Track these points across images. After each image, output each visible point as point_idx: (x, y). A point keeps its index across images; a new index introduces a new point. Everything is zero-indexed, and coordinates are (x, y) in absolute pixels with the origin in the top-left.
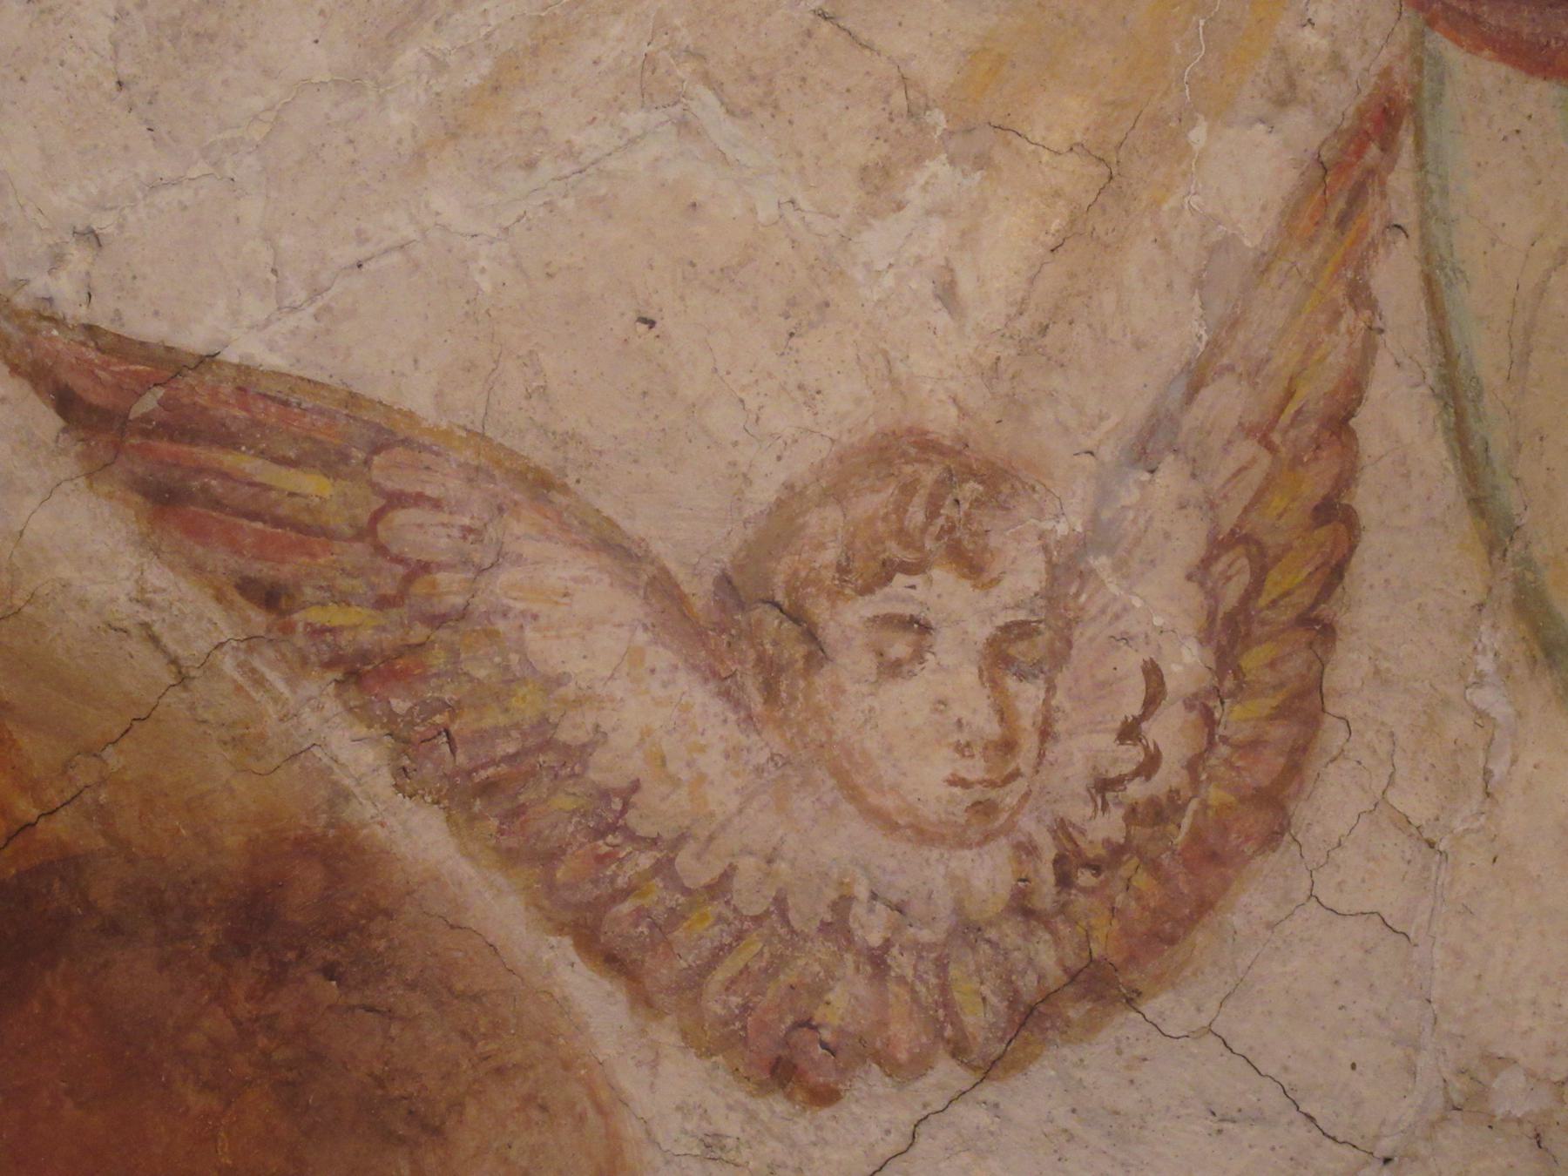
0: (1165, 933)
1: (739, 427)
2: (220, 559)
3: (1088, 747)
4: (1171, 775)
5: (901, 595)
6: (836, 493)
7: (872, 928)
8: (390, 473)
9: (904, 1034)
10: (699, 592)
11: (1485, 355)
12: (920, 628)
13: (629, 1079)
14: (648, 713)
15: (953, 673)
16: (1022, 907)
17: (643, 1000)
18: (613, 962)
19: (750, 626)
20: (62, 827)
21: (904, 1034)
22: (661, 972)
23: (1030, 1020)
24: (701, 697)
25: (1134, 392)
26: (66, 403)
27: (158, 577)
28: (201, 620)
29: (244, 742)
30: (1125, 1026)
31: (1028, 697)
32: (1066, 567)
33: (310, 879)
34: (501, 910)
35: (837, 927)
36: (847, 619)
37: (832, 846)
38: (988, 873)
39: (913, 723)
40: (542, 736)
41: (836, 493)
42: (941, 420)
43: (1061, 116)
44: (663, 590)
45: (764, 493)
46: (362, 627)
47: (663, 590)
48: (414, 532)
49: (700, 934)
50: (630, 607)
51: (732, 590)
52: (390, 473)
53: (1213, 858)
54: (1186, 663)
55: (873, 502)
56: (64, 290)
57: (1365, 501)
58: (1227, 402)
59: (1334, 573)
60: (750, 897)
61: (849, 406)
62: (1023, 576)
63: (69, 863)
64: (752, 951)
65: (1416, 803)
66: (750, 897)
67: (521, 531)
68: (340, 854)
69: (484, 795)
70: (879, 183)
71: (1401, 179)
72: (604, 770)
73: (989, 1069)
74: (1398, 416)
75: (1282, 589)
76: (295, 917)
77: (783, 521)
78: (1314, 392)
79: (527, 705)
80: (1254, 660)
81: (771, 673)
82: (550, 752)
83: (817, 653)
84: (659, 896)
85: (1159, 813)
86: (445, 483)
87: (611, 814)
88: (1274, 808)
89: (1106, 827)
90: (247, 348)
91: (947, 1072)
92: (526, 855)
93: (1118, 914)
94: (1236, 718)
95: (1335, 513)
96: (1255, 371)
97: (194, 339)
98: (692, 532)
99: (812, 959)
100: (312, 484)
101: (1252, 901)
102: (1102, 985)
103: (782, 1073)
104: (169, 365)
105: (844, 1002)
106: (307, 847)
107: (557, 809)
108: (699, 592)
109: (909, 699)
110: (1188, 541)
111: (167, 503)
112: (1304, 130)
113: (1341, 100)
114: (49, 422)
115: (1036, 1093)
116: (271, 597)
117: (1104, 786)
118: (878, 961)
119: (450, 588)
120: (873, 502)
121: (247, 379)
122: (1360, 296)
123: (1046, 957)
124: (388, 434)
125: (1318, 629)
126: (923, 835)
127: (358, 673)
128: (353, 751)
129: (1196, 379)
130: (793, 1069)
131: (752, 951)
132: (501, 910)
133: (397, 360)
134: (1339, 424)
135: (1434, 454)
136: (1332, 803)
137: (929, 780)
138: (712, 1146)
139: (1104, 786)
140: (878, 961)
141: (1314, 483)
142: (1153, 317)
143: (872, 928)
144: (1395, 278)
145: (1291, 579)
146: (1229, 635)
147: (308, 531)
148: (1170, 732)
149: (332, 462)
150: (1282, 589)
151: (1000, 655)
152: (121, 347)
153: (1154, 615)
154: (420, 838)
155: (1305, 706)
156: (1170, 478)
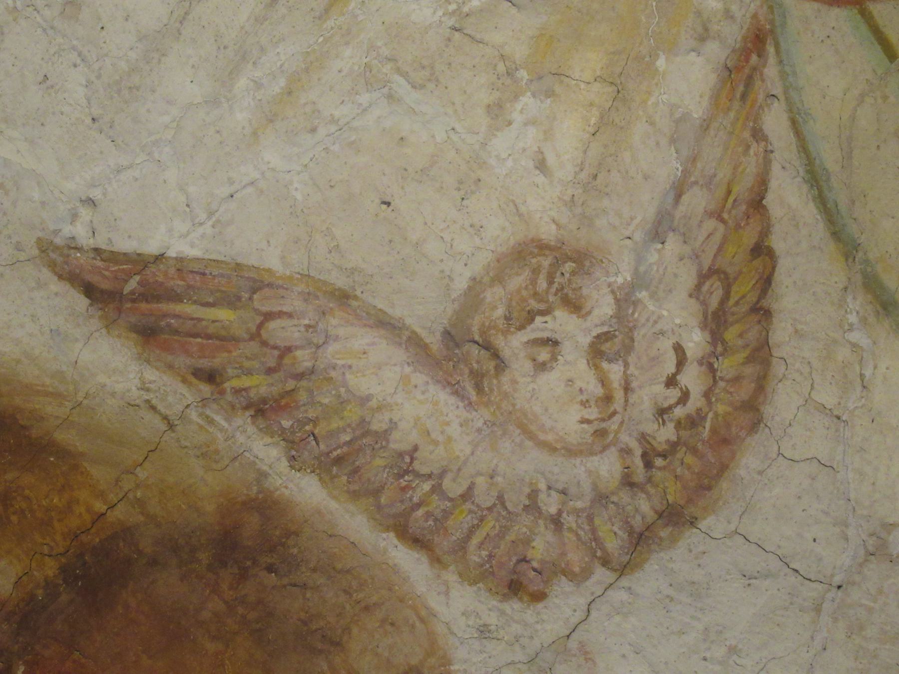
0: (705, 485)
1: (442, 252)
2: (182, 361)
3: (651, 392)
4: (696, 402)
5: (541, 327)
6: (499, 279)
7: (551, 504)
8: (263, 303)
9: (575, 558)
10: (434, 341)
11: (829, 156)
12: (553, 343)
13: (435, 602)
14: (416, 408)
15: (574, 365)
16: (628, 482)
17: (436, 561)
18: (418, 542)
19: (464, 355)
20: (119, 513)
21: (575, 558)
22: (443, 544)
23: (641, 540)
24: (443, 396)
25: (646, 205)
26: (89, 290)
27: (151, 374)
28: (177, 394)
29: (207, 454)
30: (691, 538)
31: (615, 371)
32: (625, 300)
33: (253, 521)
34: (355, 524)
35: (532, 506)
36: (513, 346)
37: (523, 465)
38: (607, 467)
39: (556, 393)
40: (363, 428)
41: (499, 279)
42: (548, 232)
43: (587, 63)
44: (415, 343)
45: (461, 284)
46: (260, 385)
47: (415, 343)
48: (281, 331)
49: (461, 520)
50: (400, 354)
51: (452, 337)
52: (263, 303)
53: (724, 440)
54: (696, 341)
55: (518, 281)
56: (80, 232)
57: (777, 242)
58: (696, 201)
59: (766, 282)
60: (484, 498)
61: (499, 232)
62: (603, 308)
63: (126, 532)
64: (490, 526)
65: (827, 396)
66: (484, 498)
67: (335, 323)
68: (266, 506)
69: (337, 465)
70: (497, 112)
71: (771, 71)
72: (399, 441)
73: (623, 570)
74: (788, 195)
75: (740, 296)
76: (248, 543)
77: (473, 297)
78: (743, 187)
79: (352, 414)
80: (731, 334)
81: (478, 378)
82: (370, 438)
83: (501, 365)
84: (436, 504)
85: (693, 422)
86: (293, 303)
87: (405, 465)
88: (752, 411)
89: (666, 434)
90: (179, 248)
91: (601, 575)
92: (364, 493)
93: (679, 479)
94: (726, 366)
95: (761, 251)
96: (709, 183)
97: (152, 248)
98: (425, 309)
99: (520, 528)
100: (224, 314)
101: (748, 462)
102: (676, 517)
103: (514, 588)
104: (141, 263)
105: (542, 546)
106: (250, 505)
107: (376, 467)
108: (434, 341)
109: (552, 380)
110: (687, 277)
111: (149, 335)
112: (716, 51)
113: (734, 33)
114: (82, 302)
115: (650, 579)
116: (211, 377)
117: (662, 412)
118: (556, 522)
119: (303, 358)
120: (518, 281)
121: (182, 265)
122: (758, 134)
123: (644, 507)
124: (260, 282)
125: (762, 313)
126: (571, 452)
127: (261, 410)
128: (266, 452)
129: (678, 191)
130: (519, 583)
131: (490, 526)
132: (355, 524)
133: (258, 241)
134: (757, 204)
135: (809, 212)
136: (783, 403)
137: (570, 422)
138: (484, 631)
139: (662, 412)
140: (556, 522)
141: (749, 237)
142: (652, 161)
143: (551, 504)
144: (775, 122)
145: (744, 288)
146: (716, 323)
147: (225, 339)
148: (692, 379)
149: (232, 301)
150: (740, 296)
151: (597, 352)
152: (114, 257)
153: (675, 318)
154: (307, 492)
155: (761, 354)
156: (673, 245)
